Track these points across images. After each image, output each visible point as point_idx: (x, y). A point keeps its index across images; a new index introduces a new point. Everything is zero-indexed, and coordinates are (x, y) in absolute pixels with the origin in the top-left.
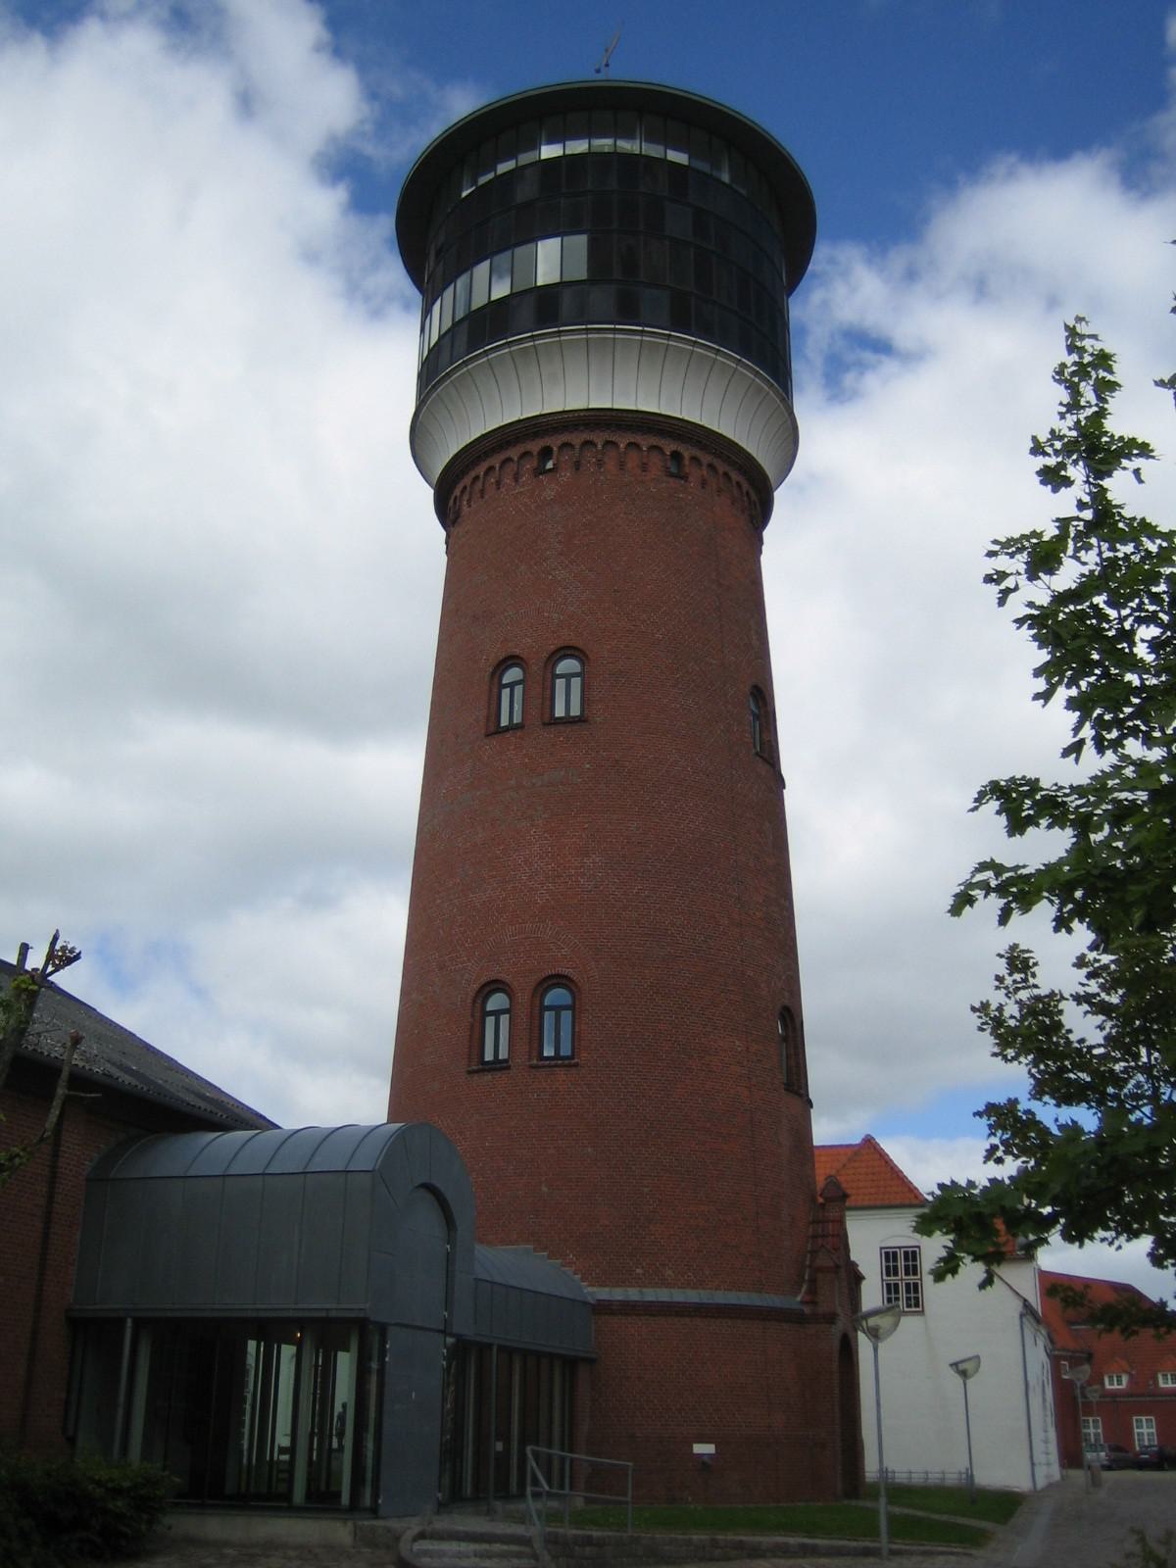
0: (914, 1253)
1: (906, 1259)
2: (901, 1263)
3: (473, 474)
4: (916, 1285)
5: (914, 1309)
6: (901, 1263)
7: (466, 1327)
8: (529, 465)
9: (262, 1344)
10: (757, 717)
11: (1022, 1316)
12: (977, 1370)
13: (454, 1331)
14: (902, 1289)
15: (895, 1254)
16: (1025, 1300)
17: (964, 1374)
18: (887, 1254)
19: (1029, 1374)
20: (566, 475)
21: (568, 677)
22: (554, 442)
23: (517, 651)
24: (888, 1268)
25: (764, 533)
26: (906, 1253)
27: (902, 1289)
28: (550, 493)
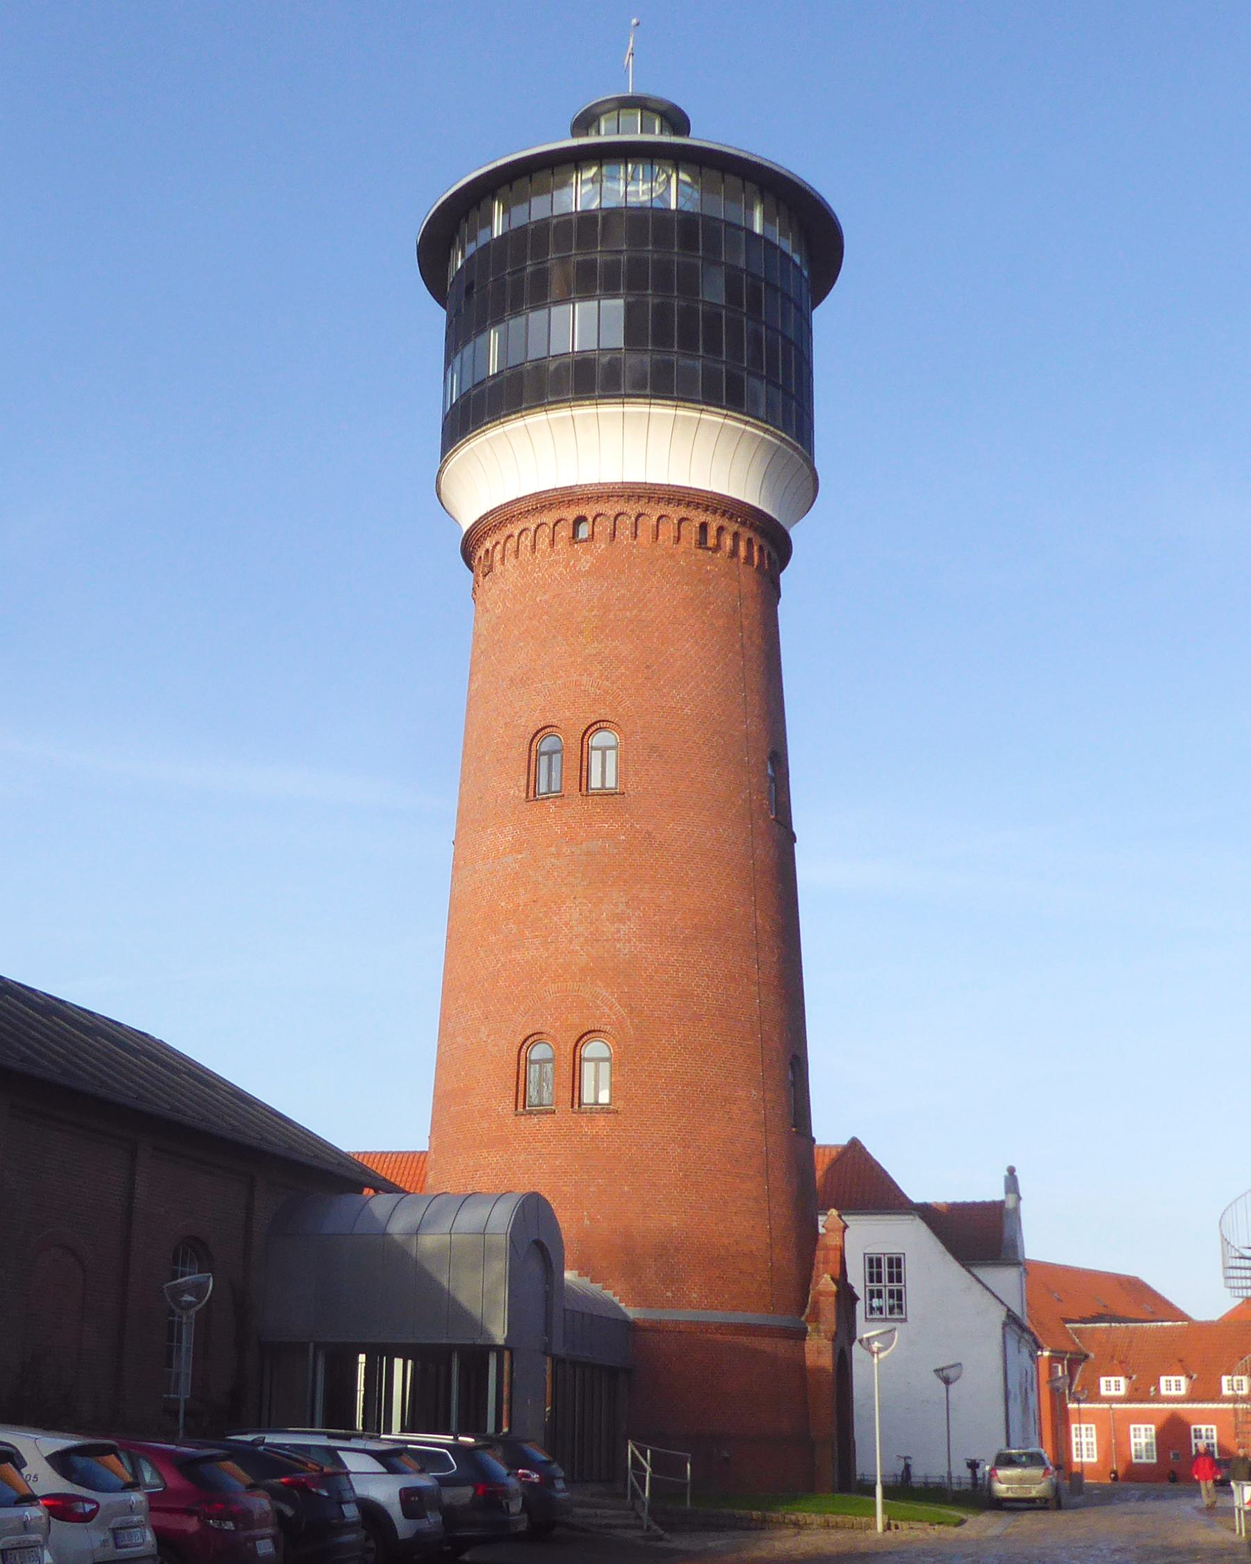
0: (899, 1260)
1: (890, 1266)
2: (885, 1270)
3: (507, 531)
4: (899, 1292)
5: (896, 1316)
6: (885, 1270)
7: (559, 1349)
8: (564, 532)
9: (410, 1362)
10: (773, 780)
11: (1005, 1325)
12: (958, 1378)
13: (554, 1352)
14: (885, 1277)
15: (879, 1260)
16: (1009, 1310)
17: (947, 1381)
18: (871, 1261)
19: (1009, 1381)
20: (601, 546)
21: (604, 750)
22: (589, 511)
23: (555, 721)
24: (871, 1274)
25: (781, 575)
26: (890, 1261)
27: (885, 1277)
28: (585, 563)
